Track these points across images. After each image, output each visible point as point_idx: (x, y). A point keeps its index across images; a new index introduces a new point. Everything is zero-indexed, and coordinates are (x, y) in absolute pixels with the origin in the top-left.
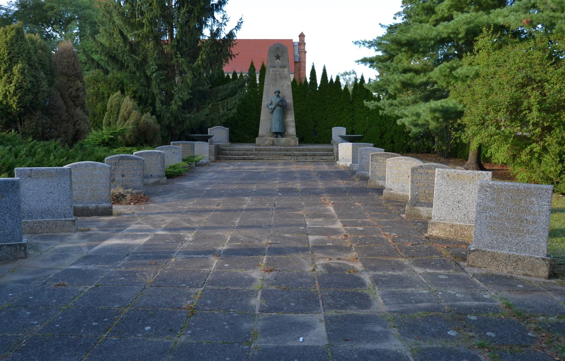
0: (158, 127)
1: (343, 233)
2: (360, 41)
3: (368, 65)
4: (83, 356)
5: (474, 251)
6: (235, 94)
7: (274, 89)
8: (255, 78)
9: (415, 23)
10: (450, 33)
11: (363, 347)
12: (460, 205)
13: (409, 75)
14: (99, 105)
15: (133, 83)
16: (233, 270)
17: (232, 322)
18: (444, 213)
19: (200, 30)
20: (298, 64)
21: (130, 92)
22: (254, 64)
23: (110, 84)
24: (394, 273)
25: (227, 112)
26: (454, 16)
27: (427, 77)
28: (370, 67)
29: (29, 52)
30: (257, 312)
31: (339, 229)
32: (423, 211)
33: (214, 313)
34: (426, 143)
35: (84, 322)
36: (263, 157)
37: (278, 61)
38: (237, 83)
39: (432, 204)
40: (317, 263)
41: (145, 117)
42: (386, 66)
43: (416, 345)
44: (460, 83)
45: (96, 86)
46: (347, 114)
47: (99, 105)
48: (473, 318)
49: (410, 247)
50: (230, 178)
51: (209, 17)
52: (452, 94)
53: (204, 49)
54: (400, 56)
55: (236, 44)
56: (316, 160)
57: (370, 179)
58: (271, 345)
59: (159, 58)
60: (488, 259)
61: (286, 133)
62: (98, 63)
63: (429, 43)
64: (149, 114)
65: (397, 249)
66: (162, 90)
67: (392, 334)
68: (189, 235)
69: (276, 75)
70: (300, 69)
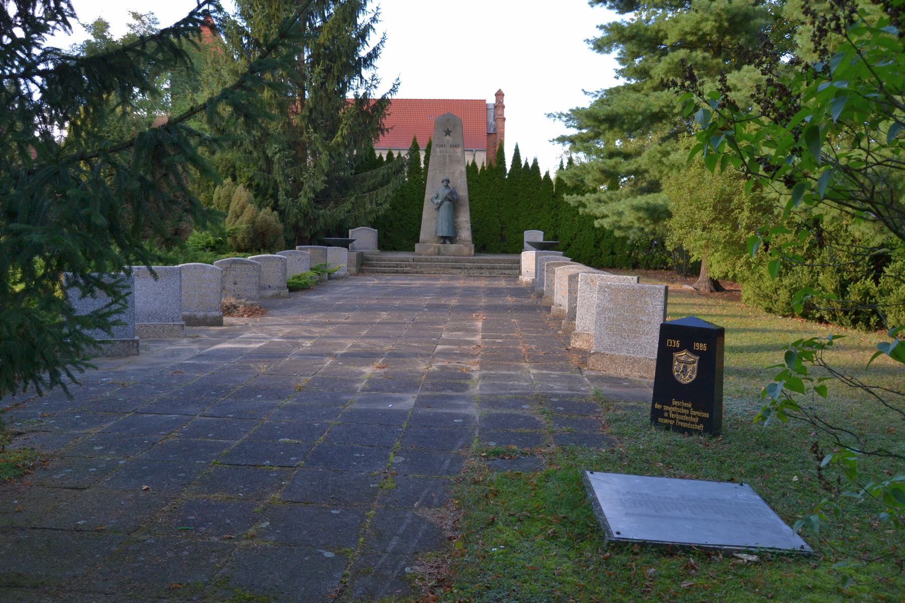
0: (281, 226)
2: (555, 114)
5: (594, 354)
6: (388, 182)
7: (441, 177)
8: (419, 160)
10: (663, 106)
13: (611, 162)
15: (248, 167)
16: (346, 367)
19: (343, 91)
20: (493, 137)
21: (244, 180)
22: (418, 142)
25: (376, 208)
29: (121, 130)
36: (422, 269)
37: (448, 137)
38: (391, 168)
41: (264, 213)
46: (548, 213)
53: (345, 122)
55: (389, 115)
56: (493, 275)
57: (546, 294)
59: (284, 133)
61: (458, 238)
63: (635, 119)
64: (268, 209)
66: (288, 176)
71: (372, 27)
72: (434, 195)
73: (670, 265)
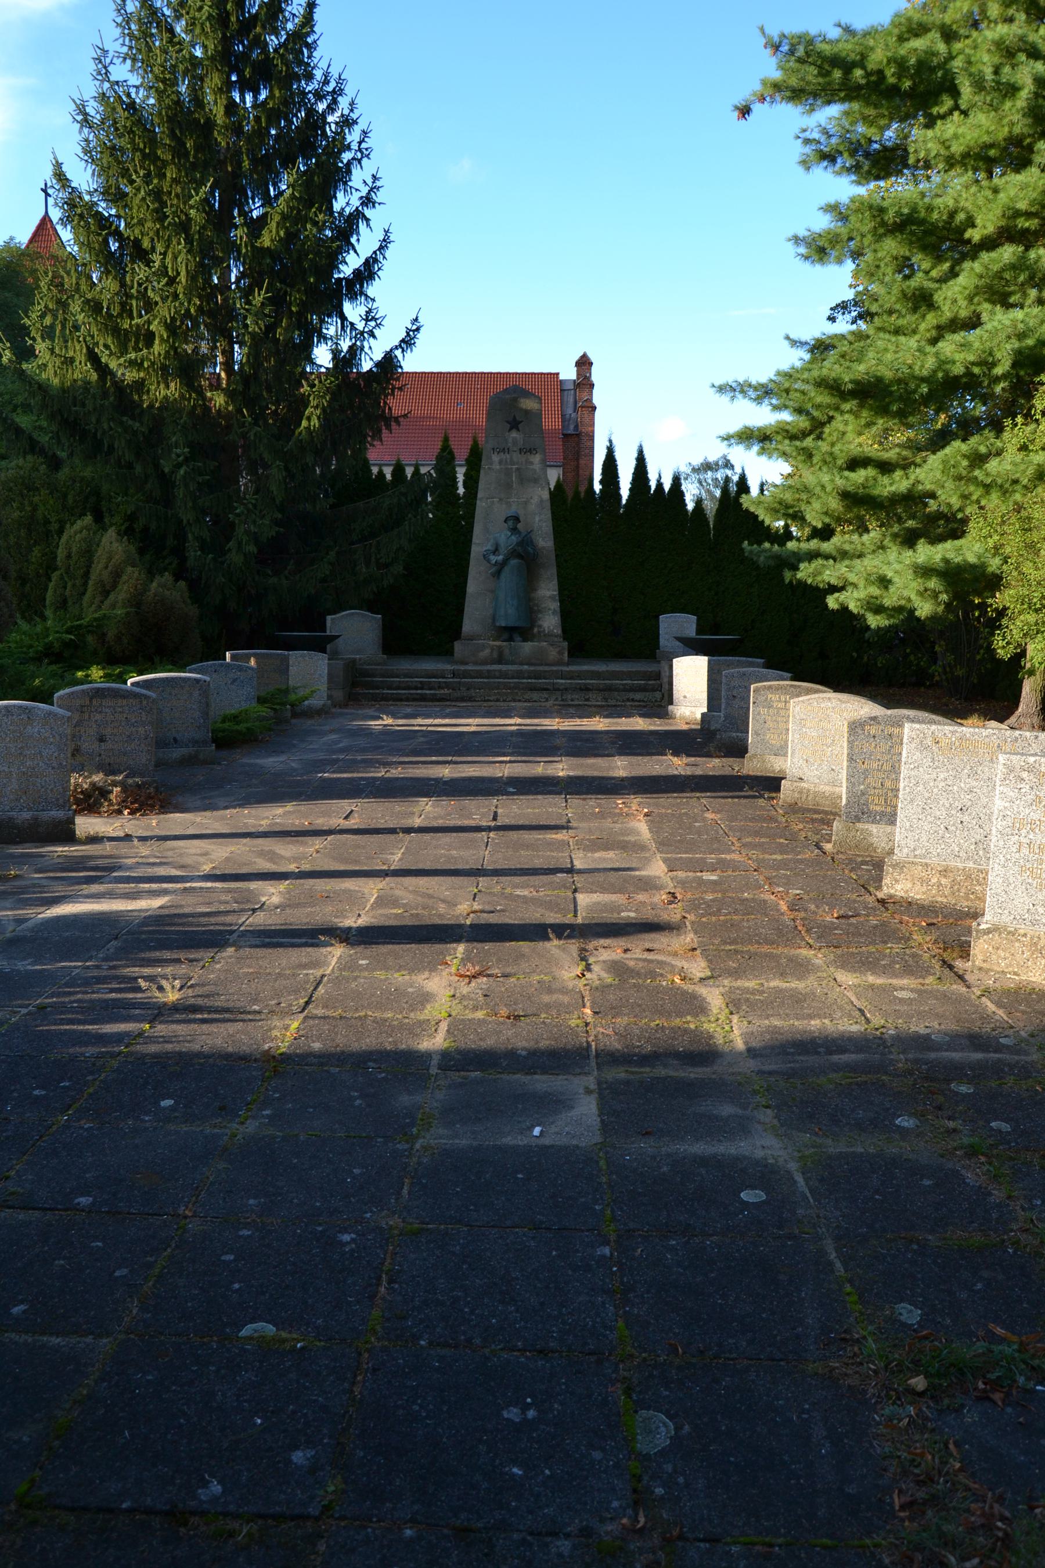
0: (193, 610)
1: (666, 888)
2: (734, 385)
3: (756, 448)
4: (15, 1162)
7: (501, 511)
8: (454, 479)
9: (882, 335)
10: (973, 364)
11: (685, 1150)
12: (966, 818)
13: (861, 475)
14: (36, 552)
15: (126, 494)
16: (380, 974)
17: (372, 1090)
18: (924, 838)
19: (305, 351)
21: (117, 519)
23: (65, 496)
24: (784, 985)
26: (985, 317)
27: (911, 481)
28: (760, 454)
30: (434, 1071)
31: (655, 877)
32: (876, 832)
33: (328, 1072)
34: (912, 657)
35: (13, 1088)
36: (472, 692)
37: (514, 434)
39: (894, 815)
40: (591, 960)
41: (159, 585)
42: (803, 449)
43: (813, 1147)
44: (995, 496)
45: (26, 502)
47: (36, 552)
48: (964, 1089)
49: (833, 923)
50: (383, 747)
51: (330, 316)
52: (974, 528)
54: (838, 424)
55: (400, 389)
56: (612, 702)
58: (464, 1142)
60: (1023, 953)
61: (536, 630)
62: (31, 438)
64: (168, 577)
65: (800, 928)
67: (759, 1122)
68: (272, 890)
69: (508, 473)
70: (577, 456)
71: (364, 216)
72: (489, 546)
73: (937, 678)
